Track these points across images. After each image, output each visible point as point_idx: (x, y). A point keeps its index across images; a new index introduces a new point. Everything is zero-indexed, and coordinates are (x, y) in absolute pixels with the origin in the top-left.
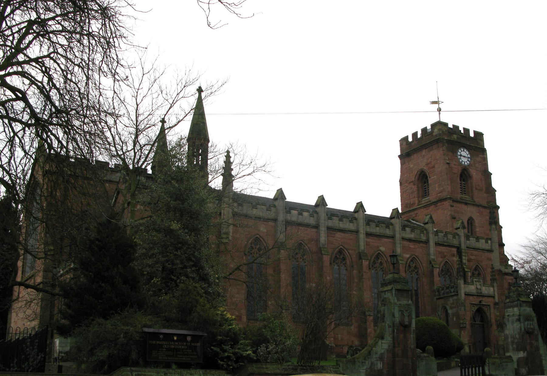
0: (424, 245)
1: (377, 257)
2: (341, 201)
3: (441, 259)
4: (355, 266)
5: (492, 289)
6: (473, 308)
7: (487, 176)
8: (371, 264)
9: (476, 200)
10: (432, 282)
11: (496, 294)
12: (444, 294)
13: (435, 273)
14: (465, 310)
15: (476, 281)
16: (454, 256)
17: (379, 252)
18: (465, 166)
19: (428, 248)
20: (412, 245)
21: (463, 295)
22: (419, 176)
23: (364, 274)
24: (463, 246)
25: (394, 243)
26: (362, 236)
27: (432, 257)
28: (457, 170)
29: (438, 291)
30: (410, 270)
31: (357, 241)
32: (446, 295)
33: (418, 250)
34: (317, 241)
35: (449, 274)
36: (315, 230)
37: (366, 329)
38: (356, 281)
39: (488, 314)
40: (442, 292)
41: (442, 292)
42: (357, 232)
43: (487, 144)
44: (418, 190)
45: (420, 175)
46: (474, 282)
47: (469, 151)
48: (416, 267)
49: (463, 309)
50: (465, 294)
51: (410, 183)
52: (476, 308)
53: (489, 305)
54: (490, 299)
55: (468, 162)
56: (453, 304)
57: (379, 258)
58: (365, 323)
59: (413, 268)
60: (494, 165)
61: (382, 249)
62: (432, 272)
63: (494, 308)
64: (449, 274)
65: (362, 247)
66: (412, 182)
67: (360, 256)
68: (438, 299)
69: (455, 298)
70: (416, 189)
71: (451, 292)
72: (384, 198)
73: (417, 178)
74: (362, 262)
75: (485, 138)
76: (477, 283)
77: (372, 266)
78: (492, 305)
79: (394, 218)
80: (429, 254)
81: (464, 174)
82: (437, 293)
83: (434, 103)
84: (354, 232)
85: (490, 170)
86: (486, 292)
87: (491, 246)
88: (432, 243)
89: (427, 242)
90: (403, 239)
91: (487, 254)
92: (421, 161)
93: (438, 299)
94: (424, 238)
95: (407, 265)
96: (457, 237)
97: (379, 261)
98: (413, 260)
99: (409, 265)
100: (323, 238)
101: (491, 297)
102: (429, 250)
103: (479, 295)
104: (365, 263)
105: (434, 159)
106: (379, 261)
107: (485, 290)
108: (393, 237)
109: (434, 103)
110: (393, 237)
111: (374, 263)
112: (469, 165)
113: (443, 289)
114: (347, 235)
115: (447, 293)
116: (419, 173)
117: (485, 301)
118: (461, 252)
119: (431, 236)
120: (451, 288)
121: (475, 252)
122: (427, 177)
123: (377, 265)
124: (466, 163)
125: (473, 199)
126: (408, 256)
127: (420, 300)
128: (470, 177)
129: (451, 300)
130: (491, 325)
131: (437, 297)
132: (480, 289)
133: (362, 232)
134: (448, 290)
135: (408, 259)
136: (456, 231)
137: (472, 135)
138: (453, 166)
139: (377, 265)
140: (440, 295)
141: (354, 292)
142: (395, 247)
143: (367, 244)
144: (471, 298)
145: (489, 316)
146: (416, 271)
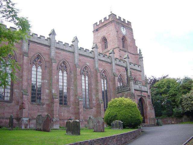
0: (110, 65)
2: (64, 37)
5: (146, 88)
7: (133, 41)
10: (114, 84)
11: (148, 90)
12: (121, 90)
20: (104, 64)
21: (133, 90)
23: (78, 76)
26: (76, 55)
29: (118, 89)
31: (74, 57)
33: (107, 68)
34: (49, 55)
36: (48, 48)
37: (79, 109)
39: (145, 101)
42: (74, 53)
43: (133, 27)
44: (102, 46)
45: (103, 39)
50: (134, 90)
52: (140, 97)
54: (146, 93)
58: (79, 105)
60: (136, 35)
61: (88, 64)
63: (148, 98)
65: (76, 61)
69: (129, 91)
72: (87, 42)
73: (101, 40)
78: (147, 97)
79: (94, 48)
80: (112, 70)
81: (124, 39)
85: (135, 38)
88: (114, 64)
89: (111, 63)
91: (139, 73)
92: (103, 33)
94: (110, 61)
95: (101, 74)
96: (125, 62)
98: (104, 72)
100: (53, 54)
101: (146, 92)
105: (110, 32)
108: (94, 58)
110: (94, 58)
114: (68, 53)
115: (124, 90)
116: (103, 37)
117: (144, 94)
119: (113, 60)
122: (106, 40)
126: (102, 69)
127: (108, 94)
134: (124, 88)
135: (102, 70)
136: (125, 60)
144: (137, 92)
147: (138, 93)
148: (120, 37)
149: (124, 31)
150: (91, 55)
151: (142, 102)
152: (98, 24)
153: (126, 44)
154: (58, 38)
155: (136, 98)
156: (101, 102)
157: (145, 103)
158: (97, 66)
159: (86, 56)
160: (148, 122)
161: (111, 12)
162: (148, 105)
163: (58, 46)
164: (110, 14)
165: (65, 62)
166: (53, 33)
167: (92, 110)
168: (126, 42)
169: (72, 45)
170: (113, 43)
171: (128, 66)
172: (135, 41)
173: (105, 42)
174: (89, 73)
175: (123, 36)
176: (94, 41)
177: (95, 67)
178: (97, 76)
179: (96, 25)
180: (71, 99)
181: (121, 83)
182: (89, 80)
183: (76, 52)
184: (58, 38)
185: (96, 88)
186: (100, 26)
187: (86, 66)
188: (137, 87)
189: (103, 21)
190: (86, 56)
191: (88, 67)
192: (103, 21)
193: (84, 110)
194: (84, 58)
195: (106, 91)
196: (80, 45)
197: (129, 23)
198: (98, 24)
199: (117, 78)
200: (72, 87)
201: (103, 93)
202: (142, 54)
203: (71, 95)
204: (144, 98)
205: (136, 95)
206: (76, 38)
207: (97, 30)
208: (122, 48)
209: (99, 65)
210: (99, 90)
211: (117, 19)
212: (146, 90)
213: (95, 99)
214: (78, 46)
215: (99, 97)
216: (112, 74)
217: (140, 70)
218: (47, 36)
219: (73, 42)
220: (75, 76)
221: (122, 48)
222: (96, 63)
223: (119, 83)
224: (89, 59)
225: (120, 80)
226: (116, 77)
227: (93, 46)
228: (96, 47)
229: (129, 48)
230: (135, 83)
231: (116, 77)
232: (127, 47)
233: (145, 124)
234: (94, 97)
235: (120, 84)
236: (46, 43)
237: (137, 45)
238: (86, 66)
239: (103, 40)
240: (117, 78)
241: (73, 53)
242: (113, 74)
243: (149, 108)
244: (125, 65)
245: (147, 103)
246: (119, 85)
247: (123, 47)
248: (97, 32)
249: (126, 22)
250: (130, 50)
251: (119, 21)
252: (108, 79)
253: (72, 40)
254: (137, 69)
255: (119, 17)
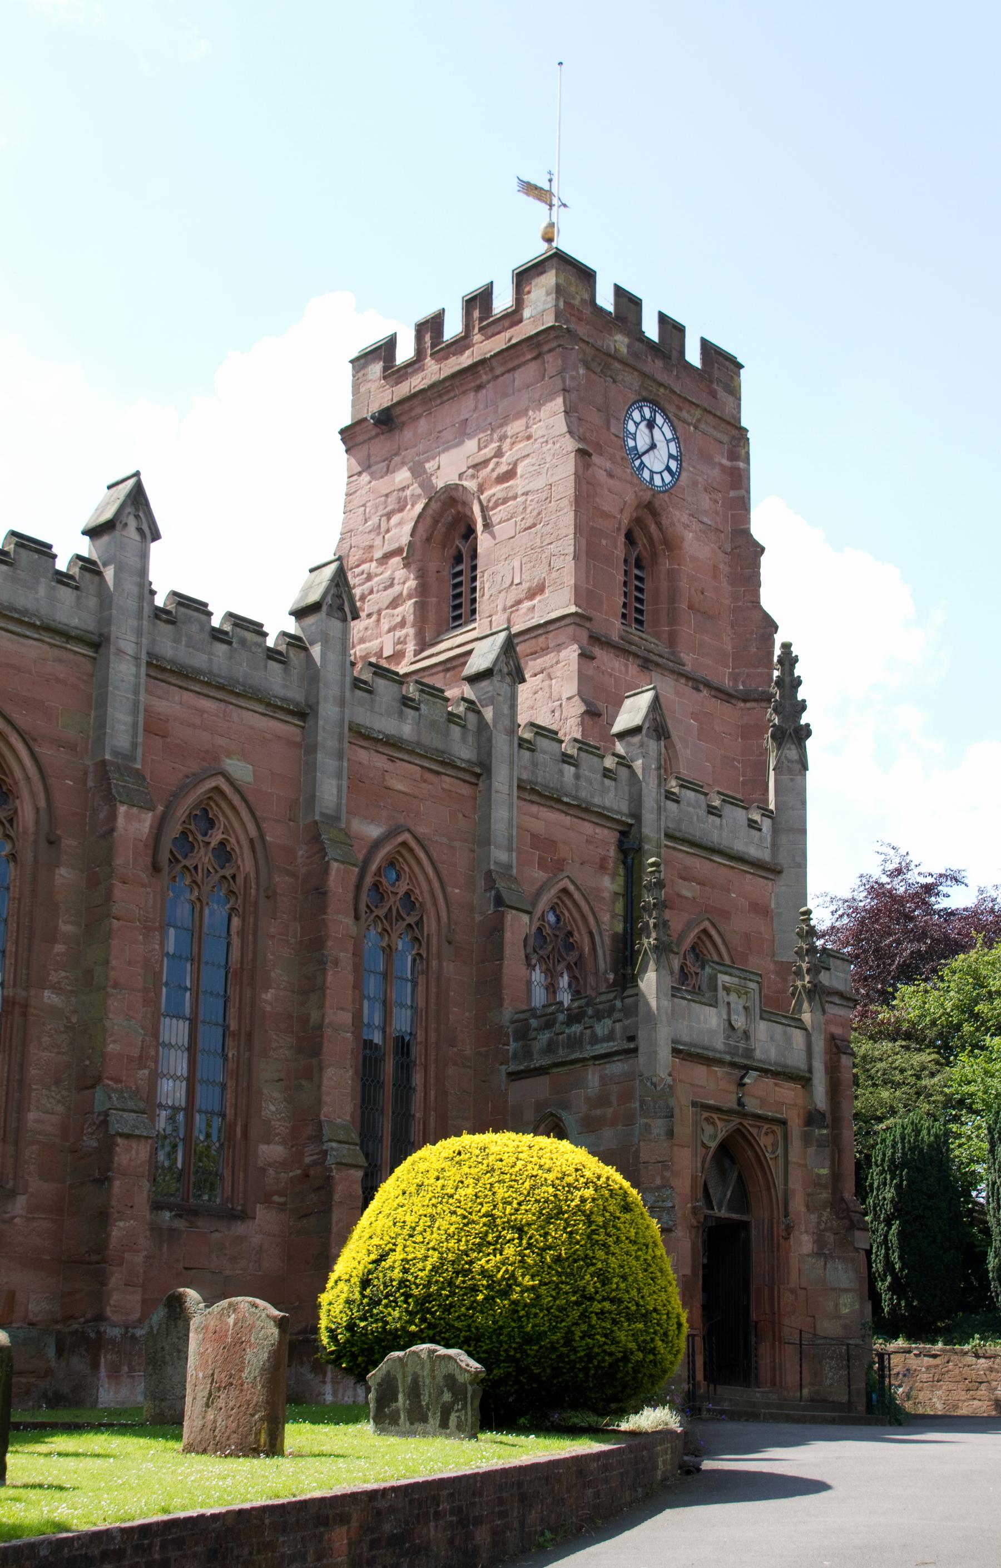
0: (465, 790)
1: (205, 818)
3: (541, 875)
4: (68, 842)
6: (709, 1130)
7: (746, 555)
8: (167, 844)
9: (688, 658)
10: (490, 985)
12: (551, 1047)
13: (508, 935)
14: (670, 1134)
15: (727, 989)
16: (602, 867)
17: (220, 782)
18: (656, 493)
19: (481, 807)
20: (401, 777)
21: (664, 1053)
22: (436, 522)
23: (119, 891)
24: (650, 827)
25: (309, 748)
26: (124, 671)
27: (499, 855)
28: (618, 503)
29: (523, 1033)
30: (381, 912)
31: (96, 699)
32: (562, 1054)
35: (572, 958)
37: (103, 1218)
38: (66, 928)
39: (776, 1170)
40: (544, 1037)
41: (544, 1037)
46: (721, 993)
47: (674, 428)
48: (409, 901)
49: (658, 1127)
50: (676, 1052)
51: (387, 556)
53: (783, 1123)
54: (788, 1093)
55: (667, 478)
56: (602, 1100)
57: (211, 824)
58: (103, 1180)
59: (393, 902)
61: (240, 769)
62: (495, 930)
63: (807, 1138)
64: (572, 958)
65: (121, 730)
66: (398, 552)
67: (108, 783)
68: (514, 1076)
69: (616, 1068)
70: (412, 583)
71: (595, 1040)
74: (113, 816)
75: (748, 381)
76: (733, 998)
77: (174, 860)
80: (482, 840)
82: (512, 1046)
83: (530, 189)
84: (79, 640)
86: (773, 1055)
87: (774, 845)
90: (361, 735)
91: (753, 885)
93: (514, 1076)
95: (369, 880)
97: (216, 837)
99: (376, 886)
102: (487, 818)
103: (742, 1065)
104: (134, 825)
106: (216, 837)
107: (768, 1041)
109: (530, 189)
110: (302, 715)
111: (185, 842)
112: (668, 490)
113: (549, 1025)
115: (575, 1042)
117: (765, 1095)
118: (639, 851)
120: (599, 1016)
121: (699, 865)
122: (470, 532)
123: (204, 858)
124: (658, 481)
125: (673, 653)
126: (374, 831)
127: (417, 1079)
128: (670, 544)
129: (593, 1078)
130: (789, 1229)
131: (513, 1067)
132: (746, 1035)
133: (129, 648)
134: (576, 1028)
135: (377, 844)
137: (693, 356)
138: (602, 476)
139: (204, 858)
140: (527, 1053)
141: (49, 997)
142: (311, 767)
143: (154, 727)
144: (700, 1072)
145: (779, 1182)
146: (411, 920)
147: (713, 1085)
148: (605, 515)
149: (655, 448)
150: (275, 680)
151: (741, 1181)
152: (405, 352)
153: (664, 585)
154: (171, 571)
155: (684, 1130)
156: (337, 1151)
157: (769, 1185)
158: (329, 791)
159: (220, 687)
160: (791, 1378)
161: (549, 240)
162: (798, 1203)
163: (168, 646)
164: (539, 249)
165: (411, 850)
166: (131, 518)
167: (240, 1228)
168: (665, 565)
169: (294, 641)
170: (532, 564)
171: (649, 817)
172: (756, 566)
173: (458, 559)
174: (246, 863)
175: (647, 496)
176: (347, 533)
177: (312, 799)
178: (316, 893)
179: (376, 369)
180: (31, 1116)
181: (564, 981)
182: (242, 933)
183: (125, 638)
184: (171, 571)
185: (304, 1020)
186: (417, 382)
187: (217, 789)
188: (707, 1023)
189: (453, 328)
190: (220, 687)
191: (236, 800)
192: (453, 328)
193: (156, 1231)
194: (205, 703)
195: (403, 1047)
196: (168, 573)
197: (722, 366)
198: (405, 352)
199: (518, 927)
200: (57, 989)
201: (369, 1058)
202: (801, 694)
203: (33, 1072)
204: (765, 1141)
205: (684, 1097)
206: (137, 498)
207: (387, 421)
208: (617, 623)
209: (360, 787)
210: (328, 1032)
211: (601, 310)
212: (796, 1059)
213: (281, 1127)
214: (143, 572)
215: (319, 1102)
216: (481, 884)
217: (765, 855)
218: (69, 546)
219: (93, 533)
220: (93, 881)
221: (615, 628)
222: (326, 762)
223: (538, 976)
224: (256, 720)
225: (555, 946)
226: (510, 915)
227: (306, 590)
228: (336, 601)
229: (688, 628)
230: (689, 983)
231: (510, 915)
232: (673, 618)
233: (757, 1394)
234: (273, 1107)
235: (552, 988)
236: (68, 610)
237: (770, 600)
238: (404, 844)
239: (441, 528)
240: (518, 927)
241: (97, 644)
242: (490, 878)
243: (804, 1243)
244: (613, 799)
245: (797, 1185)
246: (539, 997)
247: (635, 612)
248: (381, 447)
249: (693, 356)
250: (704, 649)
251: (620, 342)
252: (430, 925)
253: (96, 503)
254: (739, 846)
255: (619, 292)
